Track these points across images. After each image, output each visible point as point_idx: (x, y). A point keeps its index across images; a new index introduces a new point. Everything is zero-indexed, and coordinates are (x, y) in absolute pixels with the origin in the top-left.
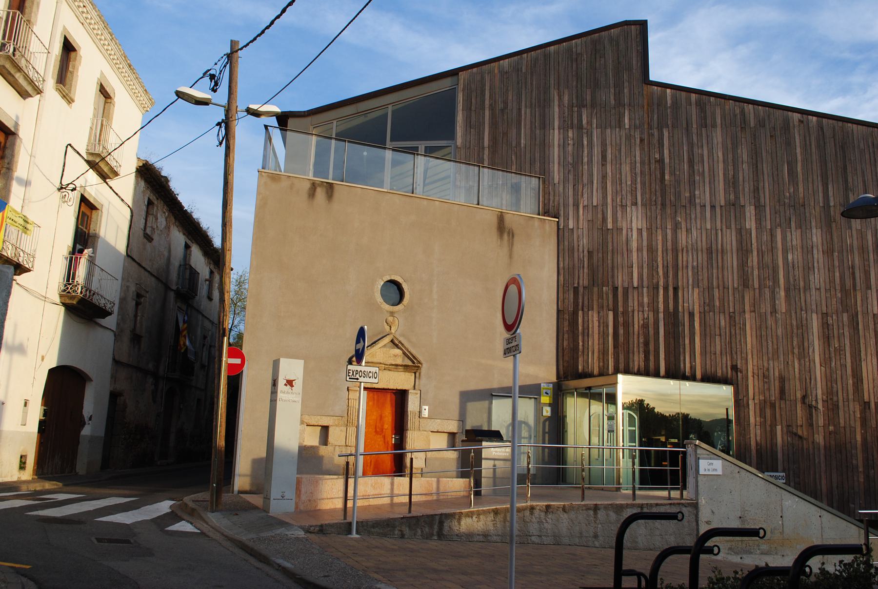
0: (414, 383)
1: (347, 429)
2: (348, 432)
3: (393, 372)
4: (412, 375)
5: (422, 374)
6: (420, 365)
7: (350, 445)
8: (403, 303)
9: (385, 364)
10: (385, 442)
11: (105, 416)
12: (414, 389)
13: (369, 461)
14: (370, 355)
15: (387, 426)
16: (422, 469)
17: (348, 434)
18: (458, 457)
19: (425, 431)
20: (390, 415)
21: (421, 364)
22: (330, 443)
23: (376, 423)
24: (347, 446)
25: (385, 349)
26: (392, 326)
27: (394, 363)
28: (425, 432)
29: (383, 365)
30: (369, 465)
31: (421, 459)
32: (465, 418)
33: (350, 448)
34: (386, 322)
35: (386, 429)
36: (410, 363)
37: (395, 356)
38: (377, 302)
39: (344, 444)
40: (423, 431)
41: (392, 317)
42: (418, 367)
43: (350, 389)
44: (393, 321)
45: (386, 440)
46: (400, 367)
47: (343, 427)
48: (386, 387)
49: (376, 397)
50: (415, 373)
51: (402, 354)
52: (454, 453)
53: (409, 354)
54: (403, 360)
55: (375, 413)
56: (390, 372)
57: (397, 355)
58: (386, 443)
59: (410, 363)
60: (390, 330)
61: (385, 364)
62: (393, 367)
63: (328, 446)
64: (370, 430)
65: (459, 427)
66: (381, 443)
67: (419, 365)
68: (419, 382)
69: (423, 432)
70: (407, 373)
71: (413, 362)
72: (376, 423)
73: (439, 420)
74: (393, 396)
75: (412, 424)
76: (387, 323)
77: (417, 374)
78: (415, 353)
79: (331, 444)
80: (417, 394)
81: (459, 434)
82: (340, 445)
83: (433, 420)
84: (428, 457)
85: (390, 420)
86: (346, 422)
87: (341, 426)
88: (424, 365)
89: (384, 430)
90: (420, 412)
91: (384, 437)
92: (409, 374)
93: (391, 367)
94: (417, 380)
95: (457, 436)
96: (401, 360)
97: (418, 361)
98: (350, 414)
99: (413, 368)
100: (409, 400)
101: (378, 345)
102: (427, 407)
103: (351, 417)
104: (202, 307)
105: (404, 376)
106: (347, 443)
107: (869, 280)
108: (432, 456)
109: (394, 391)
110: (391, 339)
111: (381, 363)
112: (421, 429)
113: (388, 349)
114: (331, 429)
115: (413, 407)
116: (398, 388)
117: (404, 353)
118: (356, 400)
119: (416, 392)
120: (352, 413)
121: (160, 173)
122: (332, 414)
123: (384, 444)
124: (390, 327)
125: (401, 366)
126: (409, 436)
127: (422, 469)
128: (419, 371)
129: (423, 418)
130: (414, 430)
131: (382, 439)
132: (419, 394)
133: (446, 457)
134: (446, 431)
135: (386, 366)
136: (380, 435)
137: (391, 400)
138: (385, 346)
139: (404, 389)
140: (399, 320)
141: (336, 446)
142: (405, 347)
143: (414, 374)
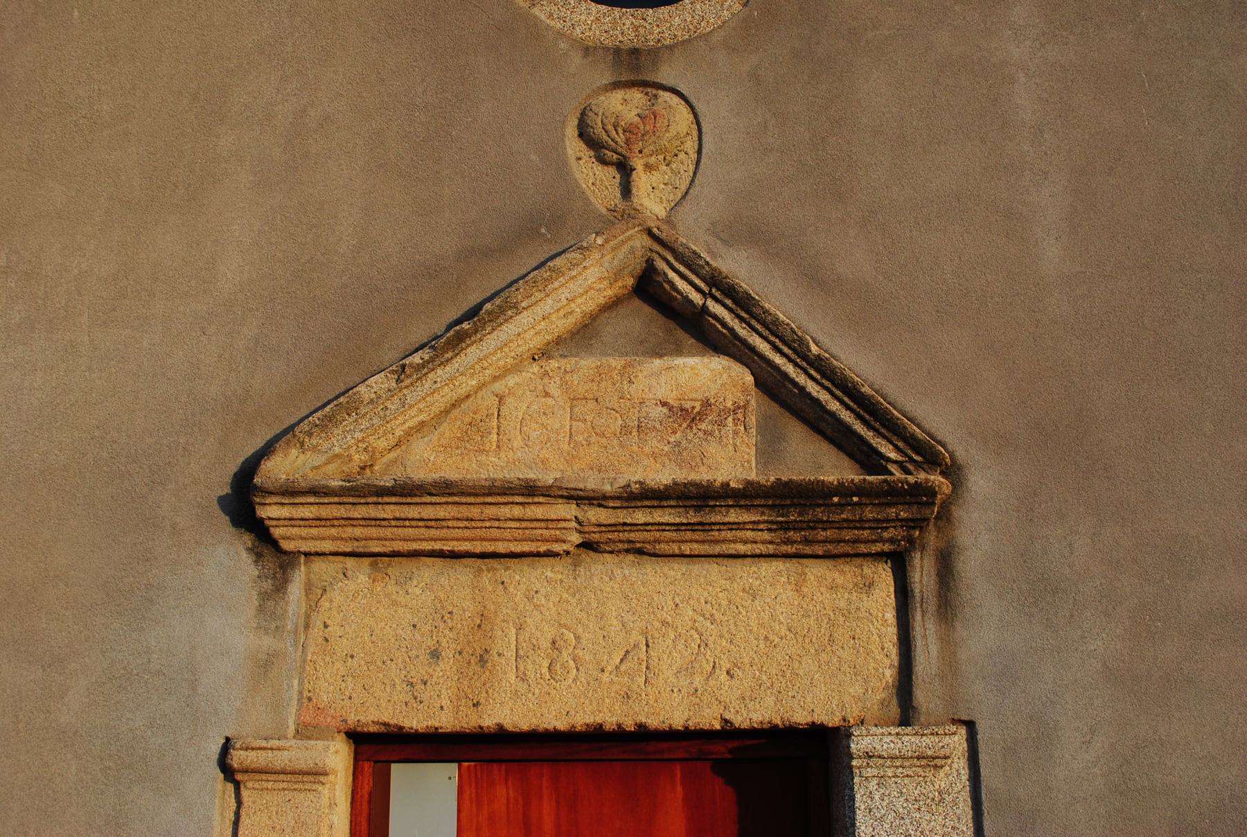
3: (675, 570)
4: (869, 586)
6: (936, 479)
11: (348, 831)
12: (906, 714)
14: (448, 430)
21: (953, 471)
25: (587, 363)
26: (638, 163)
27: (663, 475)
29: (567, 510)
34: (585, 135)
41: (636, 96)
42: (921, 494)
43: (238, 758)
44: (650, 116)
46: (733, 516)
48: (612, 715)
50: (899, 563)
51: (755, 400)
53: (812, 388)
54: (769, 450)
57: (707, 404)
60: (626, 191)
70: (816, 571)
71: (869, 460)
77: (922, 573)
78: (879, 381)
80: (933, 762)
88: (979, 483)
92: (842, 575)
93: (640, 517)
96: (749, 452)
97: (914, 444)
104: (526, 568)
105: (788, 594)
109: (720, 750)
110: (638, 265)
113: (616, 362)
119: (926, 743)
124: (624, 169)
125: (747, 495)
132: (960, 764)
139: (801, 718)
140: (700, 108)
143: (884, 576)
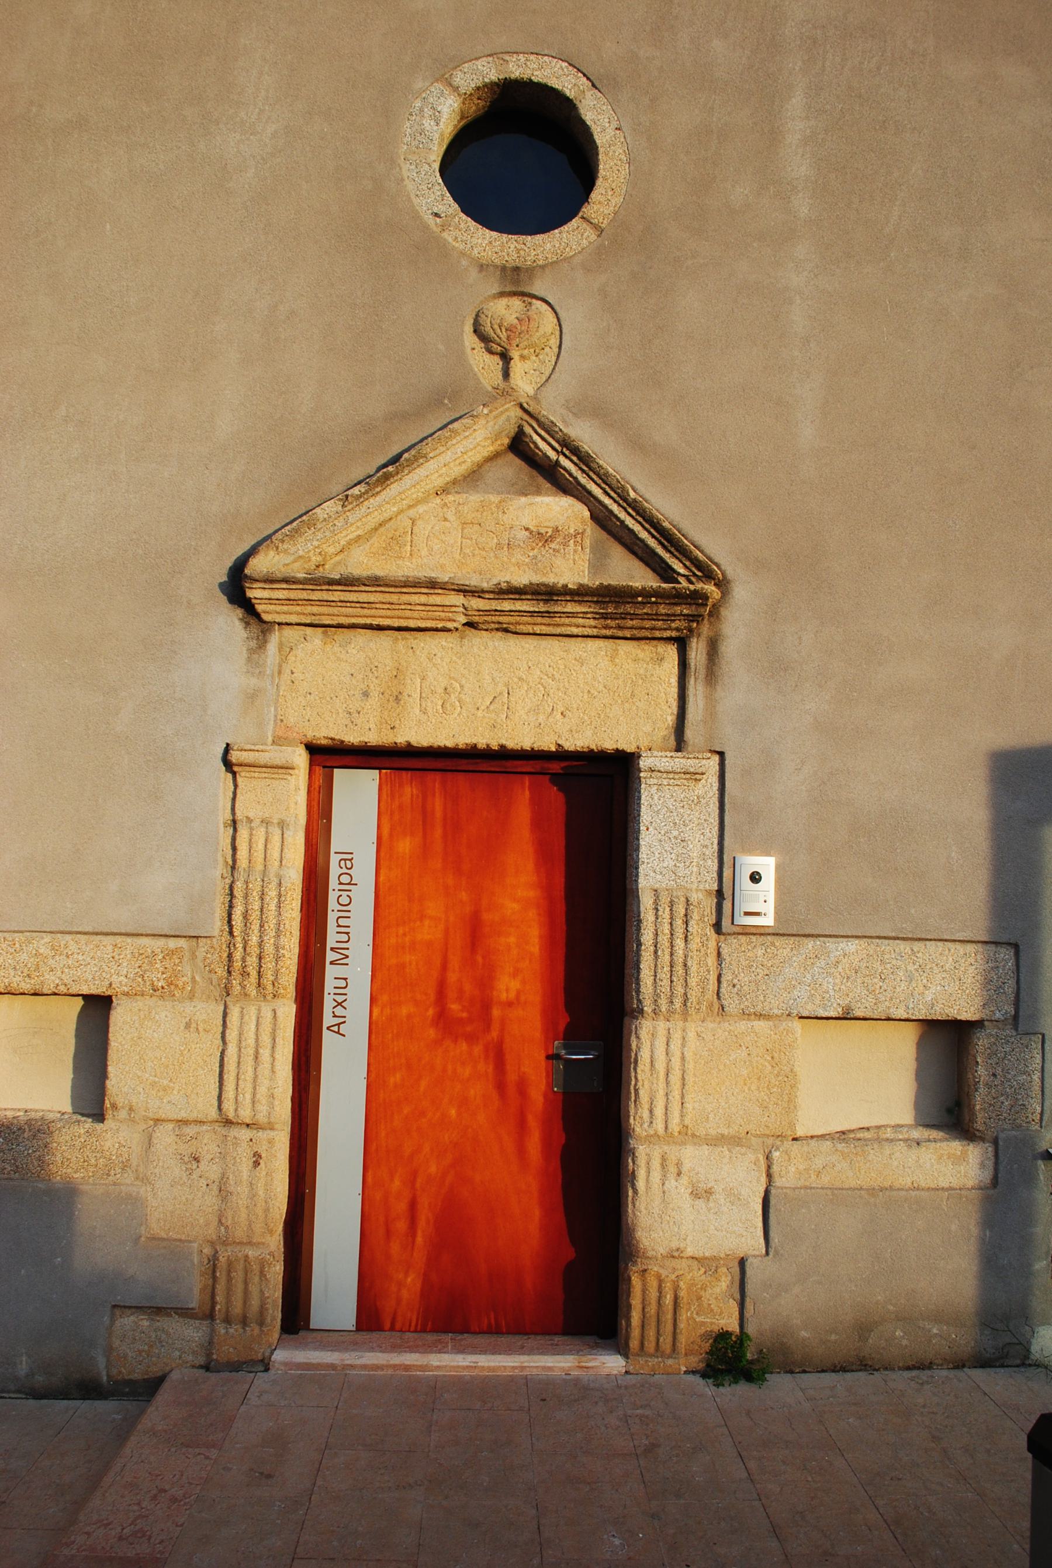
0: (674, 705)
1: (225, 1015)
2: (232, 1035)
3: (530, 643)
5: (730, 648)
6: (710, 588)
7: (246, 1114)
8: (586, 210)
9: (465, 591)
10: (501, 1086)
13: (401, 1207)
14: (377, 541)
15: (515, 985)
16: (742, 1262)
17: (232, 1050)
18: (987, 1176)
19: (760, 1016)
20: (532, 914)
21: (723, 584)
22: (114, 1106)
23: (444, 967)
24: (228, 1123)
26: (515, 354)
27: (522, 578)
28: (760, 1025)
29: (458, 599)
30: (401, 1225)
31: (734, 1197)
32: (1033, 926)
33: (244, 1134)
35: (510, 1004)
36: (642, 578)
37: (543, 538)
38: (416, 216)
39: (213, 1113)
40: (745, 1014)
41: (516, 303)
42: (697, 598)
43: (235, 756)
44: (525, 319)
45: (509, 1067)
46: (570, 608)
47: (200, 1005)
48: (485, 738)
49: (438, 805)
50: (682, 644)
51: (591, 529)
52: (963, 1158)
53: (630, 522)
54: (597, 564)
55: (434, 908)
56: (512, 640)
58: (511, 1091)
59: (642, 578)
60: (506, 375)
61: (465, 591)
62: (520, 606)
63: (109, 1123)
64: (404, 1011)
65: (990, 984)
66: (477, 1091)
67: (699, 586)
68: (711, 702)
69: (743, 1026)
71: (665, 573)
72: (444, 967)
73: (852, 946)
74: (555, 798)
75: (664, 974)
76: (484, 338)
77: (697, 652)
79: (123, 1114)
80: (694, 776)
81: (991, 1029)
82: (183, 1115)
83: (810, 943)
84: (778, 1182)
85: (535, 947)
86: (221, 972)
87: (192, 997)
88: (740, 593)
89: (496, 1012)
90: (720, 893)
91: (498, 1055)
93: (507, 606)
94: (696, 691)
95: (982, 1042)
98: (246, 916)
99: (663, 610)
100: (646, 815)
101: (420, 473)
102: (767, 865)
103: (254, 939)
106: (229, 1107)
107: (372, 1061)
108: (813, 1181)
109: (556, 767)
110: (512, 430)
111: (433, 585)
112: (732, 1004)
113: (494, 498)
114: (120, 1017)
115: (669, 863)
116: (569, 745)
117: (602, 519)
118: (282, 825)
119: (691, 764)
120: (255, 916)
121: (458, 749)
122: (122, 917)
123: (494, 1094)
124: (505, 357)
125: (580, 594)
126: (645, 1055)
127: (742, 1262)
128: (705, 629)
129: (747, 932)
130: (685, 1015)
131: (486, 1068)
133: (907, 1181)
134: (901, 1013)
135: (476, 603)
136: (471, 1039)
137: (538, 823)
138: (472, 478)
141: (157, 1121)
142: (604, 479)
143: (671, 653)
